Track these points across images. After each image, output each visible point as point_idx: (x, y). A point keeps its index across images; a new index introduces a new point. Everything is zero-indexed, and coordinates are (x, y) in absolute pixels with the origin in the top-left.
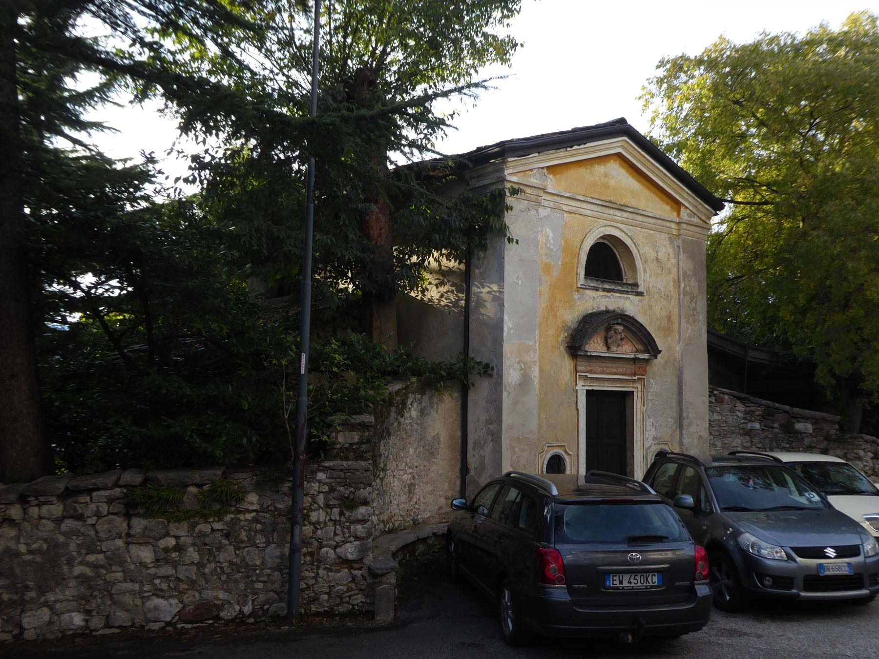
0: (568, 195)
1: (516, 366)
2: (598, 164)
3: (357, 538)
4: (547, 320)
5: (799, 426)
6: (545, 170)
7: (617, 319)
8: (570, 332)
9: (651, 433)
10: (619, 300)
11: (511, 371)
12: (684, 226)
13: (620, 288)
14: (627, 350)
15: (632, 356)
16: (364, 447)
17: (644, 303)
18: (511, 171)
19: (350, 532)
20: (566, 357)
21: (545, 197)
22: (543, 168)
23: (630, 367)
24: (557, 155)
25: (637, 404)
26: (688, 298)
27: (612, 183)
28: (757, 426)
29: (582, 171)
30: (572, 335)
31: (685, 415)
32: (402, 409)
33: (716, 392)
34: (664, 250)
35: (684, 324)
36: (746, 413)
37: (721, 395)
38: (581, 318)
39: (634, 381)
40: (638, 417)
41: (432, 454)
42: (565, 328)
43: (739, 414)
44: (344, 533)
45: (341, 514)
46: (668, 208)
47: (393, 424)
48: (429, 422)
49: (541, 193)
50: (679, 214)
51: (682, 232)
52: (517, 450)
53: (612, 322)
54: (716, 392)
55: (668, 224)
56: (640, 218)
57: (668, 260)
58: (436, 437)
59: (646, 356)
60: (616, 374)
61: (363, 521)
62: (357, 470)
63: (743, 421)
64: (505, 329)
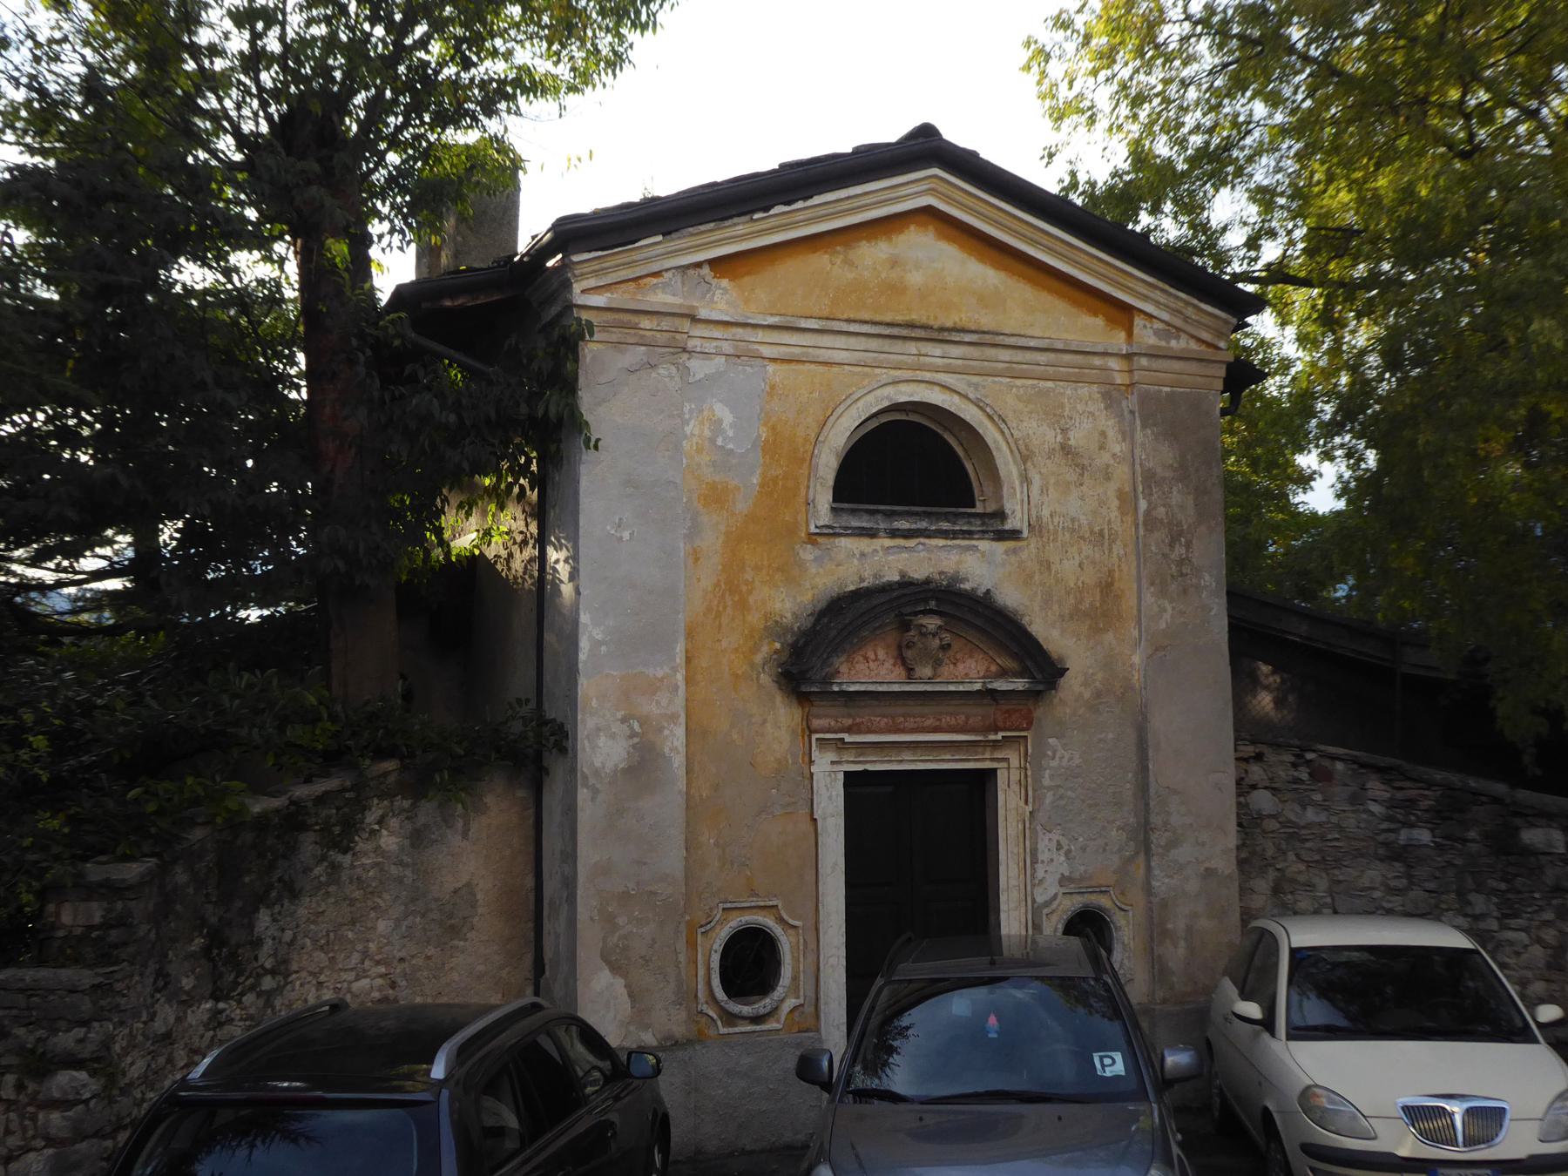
2: (869, 239)
3: (50, 1141)
4: (719, 615)
5: (1532, 836)
6: (706, 270)
7: (926, 600)
8: (790, 639)
9: (1053, 867)
10: (943, 555)
11: (602, 741)
12: (1144, 362)
13: (945, 526)
14: (969, 671)
15: (977, 687)
16: (114, 935)
17: (1024, 555)
18: (592, 283)
19: (36, 1127)
20: (779, 698)
21: (699, 331)
22: (698, 265)
23: (977, 714)
25: (1009, 804)
26: (1161, 535)
27: (915, 278)
28: (1424, 836)
29: (820, 261)
30: (794, 646)
31: (1156, 820)
32: (343, 834)
33: (1310, 756)
34: (1087, 425)
35: (1149, 599)
36: (1391, 804)
37: (1326, 763)
39: (995, 745)
40: (1012, 831)
41: (454, 931)
42: (775, 629)
43: (1376, 808)
44: (24, 1129)
45: (20, 1087)
46: (1099, 322)
47: (307, 870)
48: (471, 852)
49: (685, 325)
50: (1130, 334)
51: (1137, 376)
52: (621, 921)
53: (908, 610)
54: (1310, 756)
55: (1097, 361)
56: (1005, 355)
57: (1102, 447)
58: (466, 893)
59: (1020, 684)
60: (936, 730)
61: (63, 1104)
62: (52, 991)
63: (1385, 826)
64: (584, 644)
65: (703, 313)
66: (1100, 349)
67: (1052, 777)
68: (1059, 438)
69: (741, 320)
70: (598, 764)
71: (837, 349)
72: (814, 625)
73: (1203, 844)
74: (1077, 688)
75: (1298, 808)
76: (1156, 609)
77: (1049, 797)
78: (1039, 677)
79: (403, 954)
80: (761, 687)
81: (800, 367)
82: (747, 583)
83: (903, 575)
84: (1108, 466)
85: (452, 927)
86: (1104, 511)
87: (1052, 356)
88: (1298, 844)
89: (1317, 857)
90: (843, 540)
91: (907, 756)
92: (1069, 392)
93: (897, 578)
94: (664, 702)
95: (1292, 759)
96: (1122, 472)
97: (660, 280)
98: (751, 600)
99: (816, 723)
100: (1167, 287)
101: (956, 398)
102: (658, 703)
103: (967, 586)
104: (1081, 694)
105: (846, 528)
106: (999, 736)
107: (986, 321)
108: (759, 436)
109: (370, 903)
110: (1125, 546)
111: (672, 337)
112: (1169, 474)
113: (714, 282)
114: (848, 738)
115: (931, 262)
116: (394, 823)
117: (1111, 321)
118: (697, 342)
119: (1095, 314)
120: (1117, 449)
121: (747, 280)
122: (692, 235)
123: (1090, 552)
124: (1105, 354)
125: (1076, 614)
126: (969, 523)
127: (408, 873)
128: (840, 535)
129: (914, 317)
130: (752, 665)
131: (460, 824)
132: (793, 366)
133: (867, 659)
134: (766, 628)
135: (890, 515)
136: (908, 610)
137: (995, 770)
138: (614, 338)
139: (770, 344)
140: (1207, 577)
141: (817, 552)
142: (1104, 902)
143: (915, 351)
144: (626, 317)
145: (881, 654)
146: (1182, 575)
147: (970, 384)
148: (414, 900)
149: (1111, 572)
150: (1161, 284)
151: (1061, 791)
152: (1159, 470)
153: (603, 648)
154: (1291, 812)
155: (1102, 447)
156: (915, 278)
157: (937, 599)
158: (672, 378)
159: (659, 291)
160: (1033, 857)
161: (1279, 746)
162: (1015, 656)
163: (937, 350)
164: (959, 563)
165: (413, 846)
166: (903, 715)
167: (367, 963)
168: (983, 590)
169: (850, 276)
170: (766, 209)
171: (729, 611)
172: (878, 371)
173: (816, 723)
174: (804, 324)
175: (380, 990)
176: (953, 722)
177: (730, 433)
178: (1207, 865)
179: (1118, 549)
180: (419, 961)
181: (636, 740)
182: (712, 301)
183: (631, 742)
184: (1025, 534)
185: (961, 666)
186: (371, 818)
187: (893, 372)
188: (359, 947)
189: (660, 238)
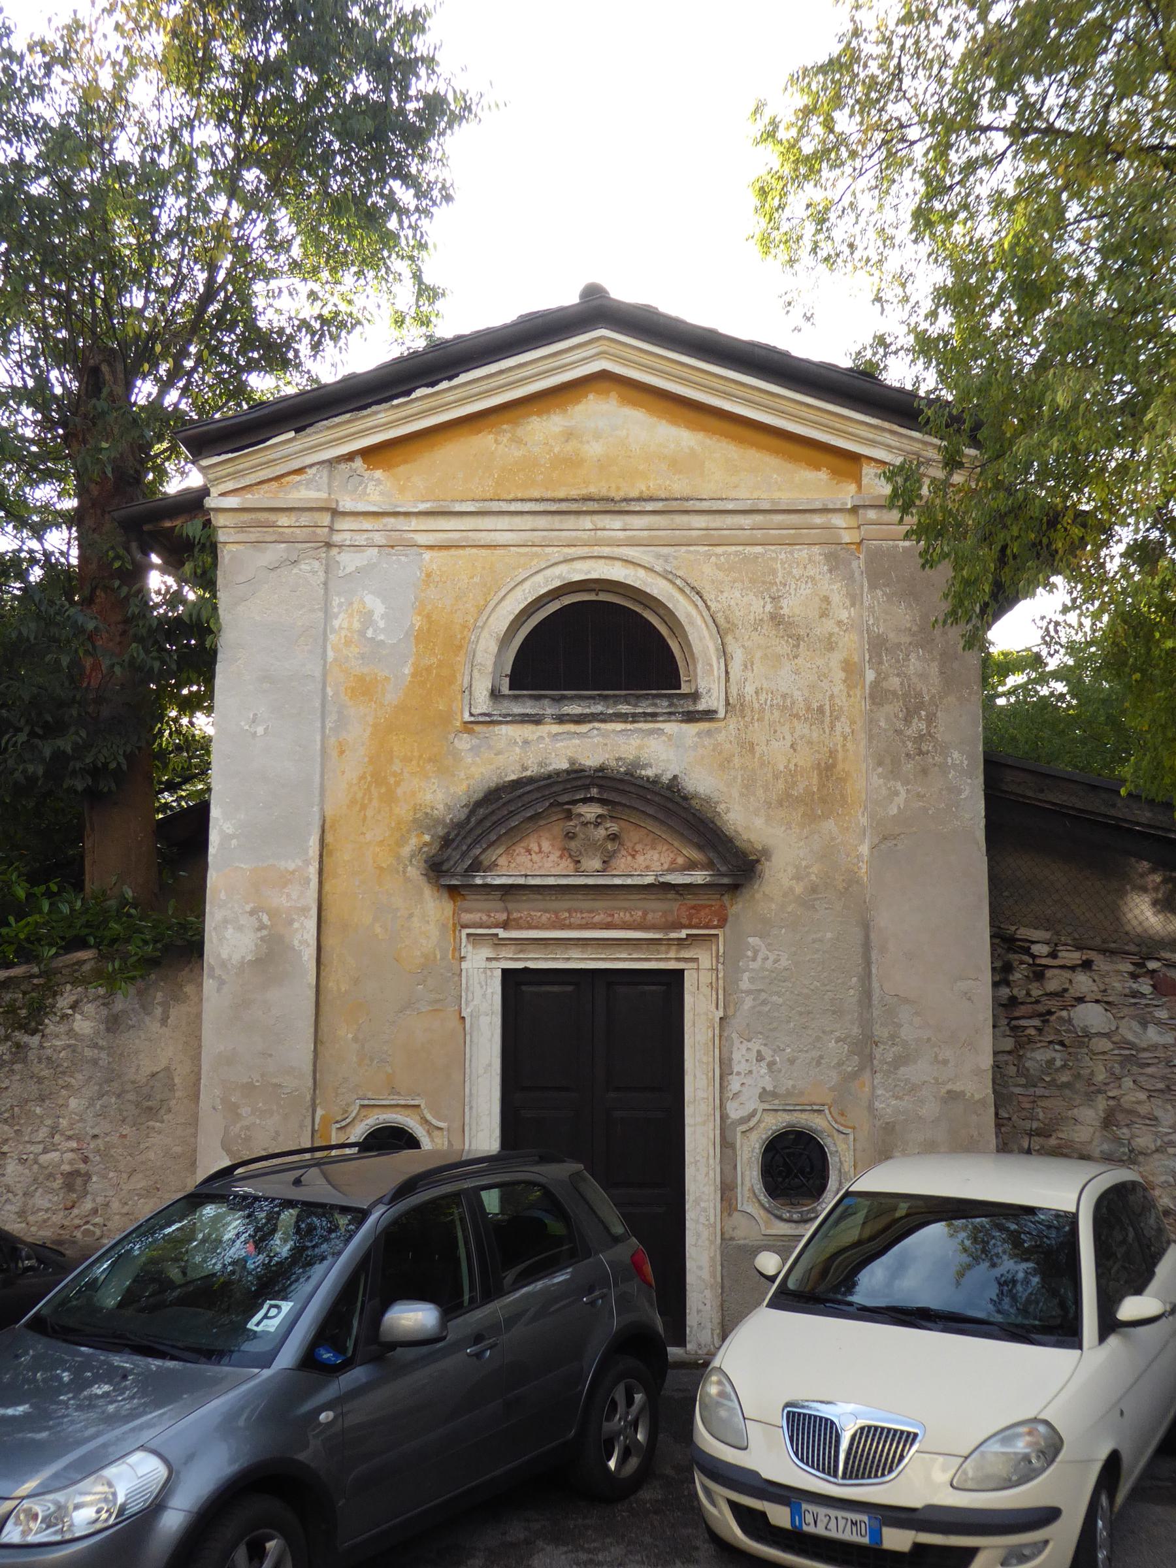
0: (422, 507)
1: (246, 921)
2: (539, 414)
4: (363, 807)
6: (358, 463)
7: (587, 787)
8: (441, 831)
10: (621, 740)
11: (230, 932)
14: (652, 860)
17: (721, 737)
18: (230, 485)
20: (428, 892)
23: (657, 908)
24: (369, 422)
26: (893, 708)
29: (484, 442)
33: (1152, 965)
34: (806, 590)
38: (479, 795)
39: (680, 943)
46: (823, 475)
52: (245, 1111)
54: (1152, 965)
55: (818, 519)
56: (700, 521)
57: (824, 614)
59: (699, 877)
60: (609, 926)
65: (347, 504)
66: (818, 505)
67: (752, 980)
68: (769, 608)
69: (389, 509)
70: (224, 956)
71: (499, 530)
72: (468, 818)
73: (945, 1062)
74: (786, 882)
75: (1135, 1025)
76: (884, 792)
77: (748, 1002)
78: (723, 869)
79: (96, 1131)
80: (407, 880)
81: (461, 552)
82: (394, 774)
83: (572, 763)
84: (831, 635)
85: (150, 1109)
86: (825, 685)
87: (759, 518)
88: (1135, 1069)
89: (1161, 1086)
90: (503, 727)
91: (575, 953)
92: (783, 556)
93: (565, 766)
94: (294, 895)
95: (1131, 968)
96: (851, 644)
97: (303, 477)
98: (399, 791)
99: (466, 917)
100: (896, 428)
101: (641, 573)
102: (288, 895)
103: (649, 772)
104: (791, 889)
105: (505, 716)
106: (683, 934)
107: (679, 486)
108: (413, 625)
109: (60, 1082)
110: (853, 723)
111: (322, 533)
112: (905, 639)
113: (367, 474)
114: (502, 933)
115: (612, 433)
116: (89, 1008)
117: (835, 472)
118: (347, 535)
119: (818, 468)
120: (844, 615)
121: (402, 469)
122: (329, 428)
123: (806, 731)
124: (825, 511)
125: (786, 800)
126: (655, 705)
127: (103, 1055)
128: (500, 723)
129: (593, 490)
130: (398, 858)
131: (158, 1011)
132: (453, 552)
133: (529, 851)
134: (415, 821)
135: (617, 699)
136: (565, 798)
137: (682, 971)
138: (252, 537)
139: (424, 532)
140: (956, 755)
141: (475, 741)
142: (817, 1122)
143: (589, 526)
144: (263, 516)
145: (546, 845)
146: (921, 753)
147: (658, 556)
148: (109, 1081)
149: (832, 753)
150: (886, 425)
151: (763, 996)
152: (892, 635)
153: (234, 842)
154: (1130, 1031)
155: (824, 614)
156: (594, 449)
157: (600, 787)
158: (314, 572)
159: (302, 488)
160: (725, 1068)
161: (1113, 952)
162: (700, 847)
163: (617, 522)
164: (640, 747)
165: (108, 1030)
166: (569, 911)
167: (57, 1137)
168: (665, 779)
169: (518, 453)
170: (408, 393)
171: (375, 803)
172: (548, 550)
173: (466, 917)
174: (458, 507)
175: (70, 1163)
176: (628, 917)
177: (382, 624)
178: (949, 1087)
179: (843, 726)
180: (114, 1139)
181: (265, 932)
182: (364, 493)
183: (259, 934)
184: (721, 714)
185: (640, 859)
186: (63, 1003)
187: (566, 550)
188: (49, 1122)
189: (292, 434)
